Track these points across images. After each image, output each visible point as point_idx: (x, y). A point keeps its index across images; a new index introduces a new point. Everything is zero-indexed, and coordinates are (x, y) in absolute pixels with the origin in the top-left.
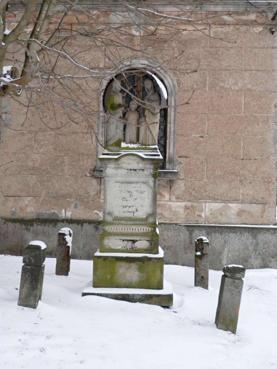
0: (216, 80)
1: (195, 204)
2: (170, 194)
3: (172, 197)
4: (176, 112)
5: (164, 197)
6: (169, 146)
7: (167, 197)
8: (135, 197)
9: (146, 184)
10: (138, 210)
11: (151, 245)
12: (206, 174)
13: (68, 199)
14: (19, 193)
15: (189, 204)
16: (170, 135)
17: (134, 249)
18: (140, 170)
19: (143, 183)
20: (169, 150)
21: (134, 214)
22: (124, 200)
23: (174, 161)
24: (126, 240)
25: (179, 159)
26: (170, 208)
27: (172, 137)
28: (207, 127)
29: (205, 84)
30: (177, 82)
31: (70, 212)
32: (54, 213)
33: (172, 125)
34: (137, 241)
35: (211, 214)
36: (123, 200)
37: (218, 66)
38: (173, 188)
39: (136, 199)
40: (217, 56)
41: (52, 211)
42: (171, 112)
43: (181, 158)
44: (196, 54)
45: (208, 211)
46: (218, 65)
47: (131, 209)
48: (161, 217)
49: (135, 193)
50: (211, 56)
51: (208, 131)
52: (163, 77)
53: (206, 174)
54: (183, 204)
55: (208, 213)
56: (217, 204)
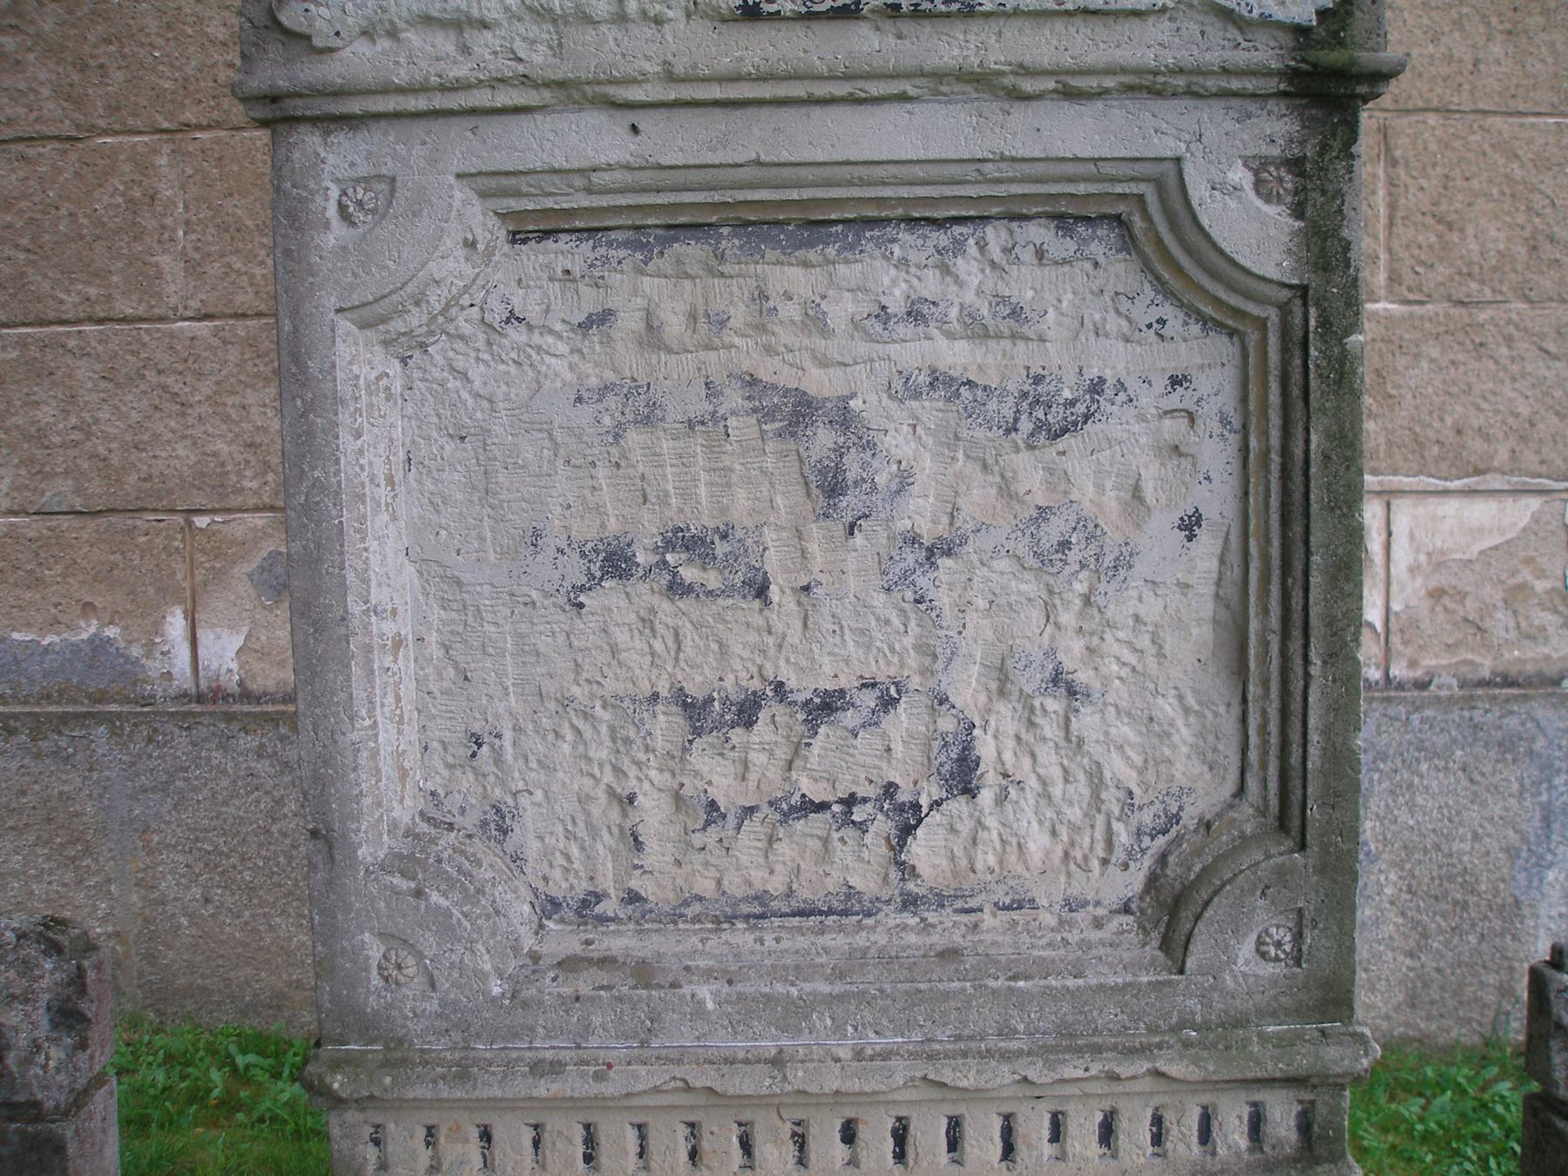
9: (1128, 242)
10: (985, 748)
13: (201, 522)
19: (1061, 222)
21: (924, 849)
22: (713, 580)
31: (233, 627)
32: (98, 645)
35: (1437, 594)
36: (678, 588)
39: (935, 552)
41: (88, 630)
45: (1413, 570)
53: (1383, 256)
56: (1481, 511)
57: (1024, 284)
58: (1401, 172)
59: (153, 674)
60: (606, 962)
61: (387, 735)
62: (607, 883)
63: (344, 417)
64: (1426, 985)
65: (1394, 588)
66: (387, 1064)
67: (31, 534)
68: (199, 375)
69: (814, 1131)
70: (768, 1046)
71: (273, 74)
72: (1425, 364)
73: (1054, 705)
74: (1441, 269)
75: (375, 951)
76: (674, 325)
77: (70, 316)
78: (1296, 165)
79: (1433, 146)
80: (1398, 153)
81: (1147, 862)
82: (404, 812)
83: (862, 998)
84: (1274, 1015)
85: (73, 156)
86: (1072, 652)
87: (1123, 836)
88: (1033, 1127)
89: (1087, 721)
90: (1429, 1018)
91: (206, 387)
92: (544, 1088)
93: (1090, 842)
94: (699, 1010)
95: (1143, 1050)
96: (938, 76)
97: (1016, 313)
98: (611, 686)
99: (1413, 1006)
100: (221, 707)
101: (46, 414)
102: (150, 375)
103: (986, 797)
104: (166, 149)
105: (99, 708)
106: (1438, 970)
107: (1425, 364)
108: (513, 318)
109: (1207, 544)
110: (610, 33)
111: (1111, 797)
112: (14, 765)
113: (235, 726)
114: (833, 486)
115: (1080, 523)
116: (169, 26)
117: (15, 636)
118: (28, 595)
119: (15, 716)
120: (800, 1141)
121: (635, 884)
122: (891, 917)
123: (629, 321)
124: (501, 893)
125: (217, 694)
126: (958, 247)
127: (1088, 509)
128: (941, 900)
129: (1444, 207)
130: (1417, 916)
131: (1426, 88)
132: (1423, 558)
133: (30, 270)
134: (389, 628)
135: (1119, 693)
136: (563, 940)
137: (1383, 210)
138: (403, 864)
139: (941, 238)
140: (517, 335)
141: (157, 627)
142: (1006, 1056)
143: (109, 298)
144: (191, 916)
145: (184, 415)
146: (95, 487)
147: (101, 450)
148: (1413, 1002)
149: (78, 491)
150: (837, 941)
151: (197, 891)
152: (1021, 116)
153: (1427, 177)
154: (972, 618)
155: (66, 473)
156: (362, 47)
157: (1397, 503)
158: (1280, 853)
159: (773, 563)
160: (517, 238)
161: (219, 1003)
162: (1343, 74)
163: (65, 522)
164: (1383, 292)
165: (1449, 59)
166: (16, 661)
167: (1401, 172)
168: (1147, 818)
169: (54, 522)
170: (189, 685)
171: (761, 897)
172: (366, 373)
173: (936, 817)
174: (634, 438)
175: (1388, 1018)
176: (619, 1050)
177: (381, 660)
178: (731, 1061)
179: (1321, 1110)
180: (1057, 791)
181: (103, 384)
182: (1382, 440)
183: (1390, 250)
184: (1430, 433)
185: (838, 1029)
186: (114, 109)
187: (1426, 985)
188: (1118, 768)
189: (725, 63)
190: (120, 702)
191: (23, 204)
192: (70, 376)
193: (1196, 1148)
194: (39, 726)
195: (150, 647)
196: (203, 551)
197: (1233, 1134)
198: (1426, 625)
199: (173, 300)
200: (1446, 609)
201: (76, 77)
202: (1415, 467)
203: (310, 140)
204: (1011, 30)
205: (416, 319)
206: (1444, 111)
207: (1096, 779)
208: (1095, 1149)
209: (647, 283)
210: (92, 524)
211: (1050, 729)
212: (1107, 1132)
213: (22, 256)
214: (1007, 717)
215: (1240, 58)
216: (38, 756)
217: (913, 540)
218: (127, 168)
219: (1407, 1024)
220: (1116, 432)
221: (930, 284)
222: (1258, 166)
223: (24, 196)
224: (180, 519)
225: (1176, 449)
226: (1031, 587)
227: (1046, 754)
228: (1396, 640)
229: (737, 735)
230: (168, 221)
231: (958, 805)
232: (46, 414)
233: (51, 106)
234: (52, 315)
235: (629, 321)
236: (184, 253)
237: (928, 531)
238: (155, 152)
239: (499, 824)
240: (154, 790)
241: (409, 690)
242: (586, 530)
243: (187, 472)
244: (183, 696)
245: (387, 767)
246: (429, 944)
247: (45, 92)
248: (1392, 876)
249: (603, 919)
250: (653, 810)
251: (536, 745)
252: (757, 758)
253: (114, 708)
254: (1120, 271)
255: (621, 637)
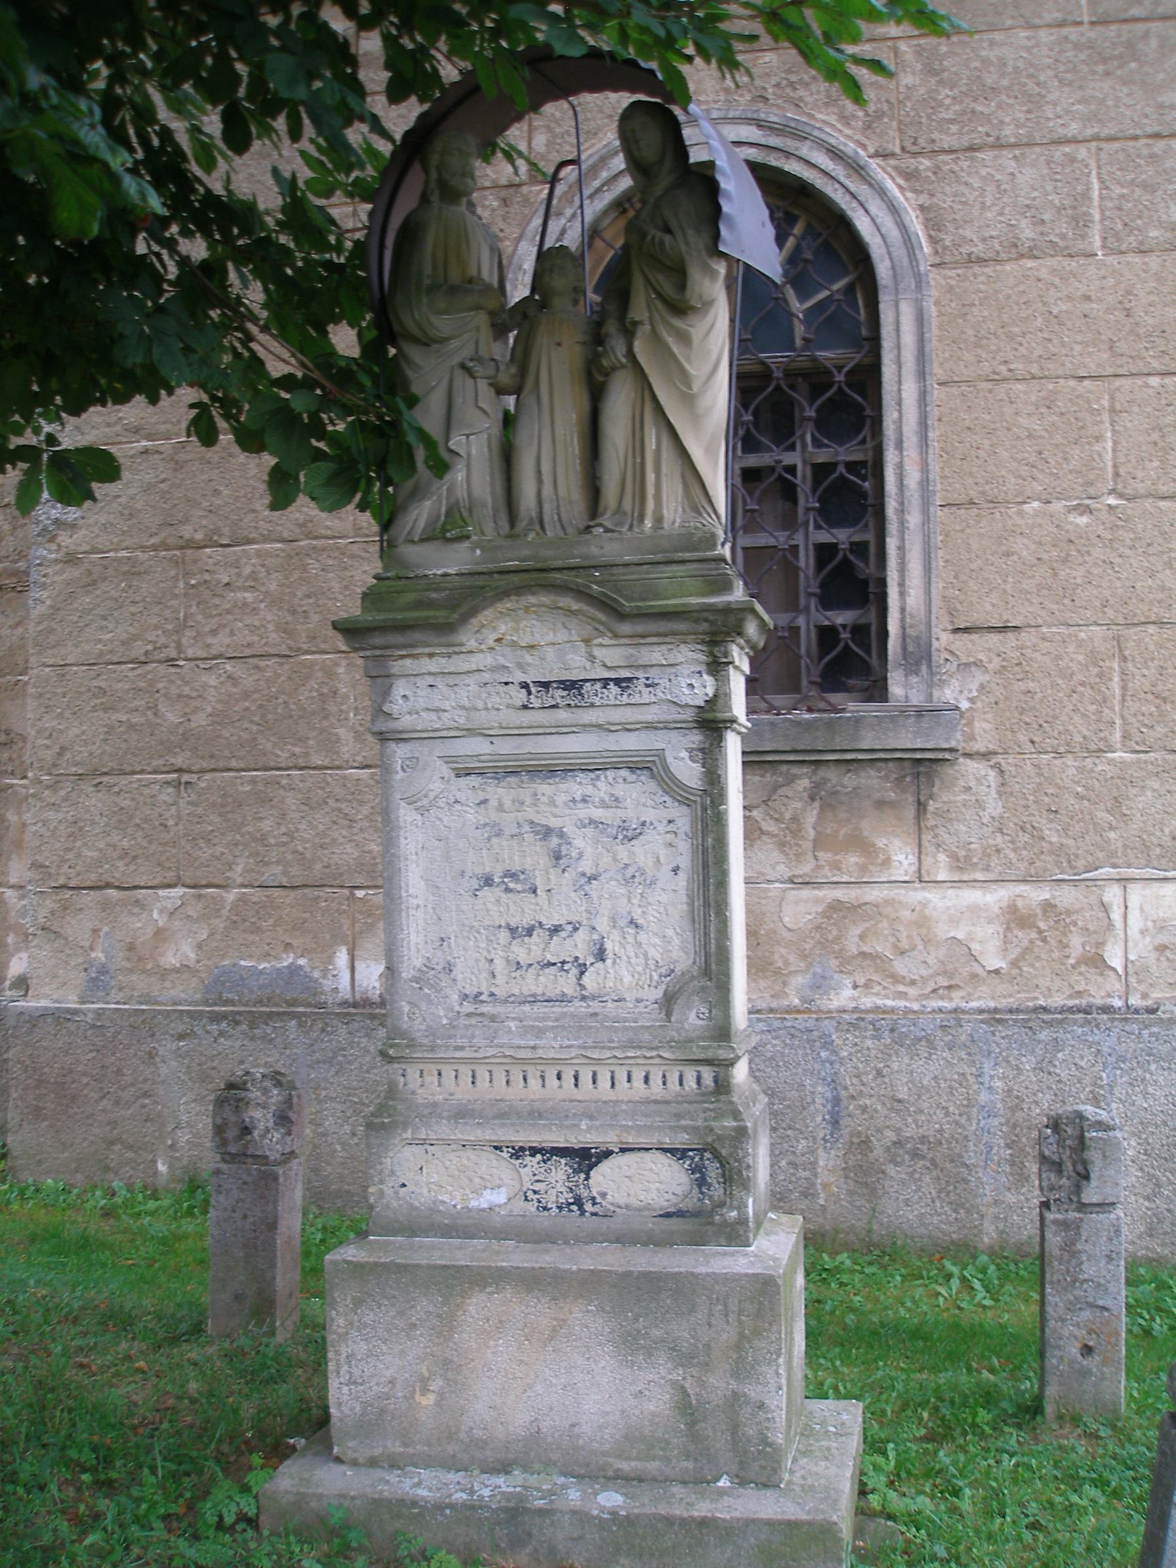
0: (1138, 192)
1: (1065, 897)
2: (920, 846)
3: (928, 861)
4: (929, 381)
5: (887, 862)
6: (902, 570)
7: (903, 860)
8: (587, 866)
9: (653, 777)
10: (609, 945)
11: (702, 1182)
12: (1118, 721)
13: (360, 894)
14: (120, 871)
15: (1037, 895)
16: (901, 511)
17: (588, 1207)
18: (605, 682)
20: (902, 594)
21: (587, 979)
22: (519, 887)
23: (934, 658)
24: (534, 1151)
25: (961, 643)
26: (923, 922)
27: (914, 519)
28: (1109, 456)
29: (1081, 222)
30: (927, 220)
32: (294, 970)
33: (911, 452)
34: (608, 1154)
35: (1161, 949)
36: (508, 890)
37: (1146, 116)
38: (932, 806)
39: (592, 878)
40: (1133, 65)
41: (287, 960)
42: (900, 382)
43: (974, 637)
44: (1021, 65)
45: (1143, 932)
46: (1148, 110)
47: (560, 949)
48: (875, 977)
49: (581, 841)
50: (1100, 68)
51: (1117, 474)
52: (848, 197)
53: (1118, 721)
54: (995, 898)
55: (1142, 948)
57: (620, 790)
58: (1130, 665)
59: (327, 989)
60: (482, 1014)
61: (413, 937)
62: (483, 989)
63: (402, 833)
64: (1160, 1221)
65: (1130, 944)
66: (408, 1046)
67: (255, 899)
68: (362, 803)
69: (547, 1075)
70: (532, 1043)
71: (381, 726)
72: (1149, 793)
73: (631, 931)
74: (1158, 729)
75: (406, 1008)
76: (508, 804)
77: (283, 765)
78: (702, 750)
79: (1152, 647)
80: (1127, 653)
81: (664, 987)
82: (418, 963)
83: (563, 1027)
84: (703, 1039)
85: (287, 667)
86: (637, 913)
87: (656, 977)
88: (622, 1076)
89: (642, 937)
90: (1163, 1245)
91: (365, 810)
92: (458, 1054)
93: (645, 979)
94: (510, 1031)
95: (656, 1048)
96: (585, 726)
97: (617, 800)
98: (487, 922)
99: (1151, 1236)
100: (368, 1011)
101: (267, 825)
102: (331, 802)
103: (609, 962)
104: (344, 663)
105: (291, 1009)
106: (1169, 1210)
107: (1149, 793)
108: (456, 802)
109: (682, 878)
110: (484, 713)
111: (651, 962)
112: (238, 1043)
113: (376, 1022)
114: (558, 857)
115: (639, 869)
116: (346, 588)
117: (242, 963)
118: (251, 937)
119: (239, 1013)
120: (543, 1078)
121: (493, 990)
122: (577, 1003)
123: (493, 803)
124: (449, 991)
125: (366, 1003)
126: (598, 778)
127: (641, 864)
128: (594, 998)
129: (1160, 687)
130: (1152, 1171)
131: (1146, 608)
132: (1150, 924)
133: (259, 737)
134: (415, 901)
135: (654, 927)
136: (468, 1007)
137: (1117, 691)
138: (416, 980)
139: (592, 775)
140: (458, 807)
141: (330, 960)
142: (609, 1048)
143: (307, 754)
144: (343, 1144)
145: (351, 827)
146: (295, 871)
147: (300, 848)
148: (1151, 1232)
149: (285, 873)
150: (557, 1010)
151: (347, 1128)
152: (612, 736)
153: (1148, 668)
154: (604, 901)
155: (278, 862)
156: (408, 717)
157: (1131, 887)
158: (704, 982)
159: (539, 882)
160: (458, 776)
161: (358, 1202)
162: (714, 721)
163: (276, 892)
164: (1119, 746)
165: (1163, 588)
166: (242, 979)
167: (1130, 665)
168: (663, 971)
169: (269, 892)
170: (348, 996)
171: (534, 995)
172: (410, 819)
173: (591, 969)
174: (494, 840)
175: (1133, 1243)
176: (483, 1043)
177: (412, 912)
178: (519, 1047)
179: (722, 1075)
180: (633, 961)
181: (303, 807)
182: (1120, 844)
183: (1123, 717)
184: (1154, 839)
185: (555, 1039)
186: (312, 638)
187: (1160, 1221)
188: (653, 953)
189: (518, 723)
190: (305, 1006)
191: (256, 696)
192: (282, 802)
193: (678, 1088)
194: (254, 1020)
195: (325, 972)
196: (361, 912)
197: (691, 1083)
198: (1154, 969)
199: (346, 756)
200: (1168, 959)
201: (290, 619)
202: (1143, 862)
203: (392, 745)
204: (607, 710)
205: (425, 802)
206: (1160, 623)
207: (646, 958)
208: (642, 1086)
209: (500, 790)
210: (292, 894)
211: (630, 939)
212: (646, 1079)
213: (255, 728)
214: (616, 935)
215: (679, 717)
216: (252, 1039)
217: (584, 874)
218: (320, 674)
219: (1147, 1248)
220: (650, 838)
221: (589, 790)
222: (690, 750)
223: (256, 691)
224: (346, 892)
225: (671, 845)
226: (623, 891)
227: (629, 948)
228: (1132, 980)
229: (526, 939)
230: (344, 707)
231: (600, 965)
232: (267, 825)
233: (274, 635)
234: (272, 764)
235: (493, 803)
236: (353, 728)
237: (589, 872)
238: (337, 665)
239: (449, 968)
240: (324, 1062)
241: (421, 922)
242: (479, 871)
243: (352, 862)
244: (345, 1003)
245: (413, 948)
246: (423, 1005)
247: (271, 627)
248: (1133, 1143)
249: (482, 1002)
250: (499, 965)
251: (461, 942)
252: (534, 948)
253: (301, 1009)
254: (652, 785)
255: (490, 906)
